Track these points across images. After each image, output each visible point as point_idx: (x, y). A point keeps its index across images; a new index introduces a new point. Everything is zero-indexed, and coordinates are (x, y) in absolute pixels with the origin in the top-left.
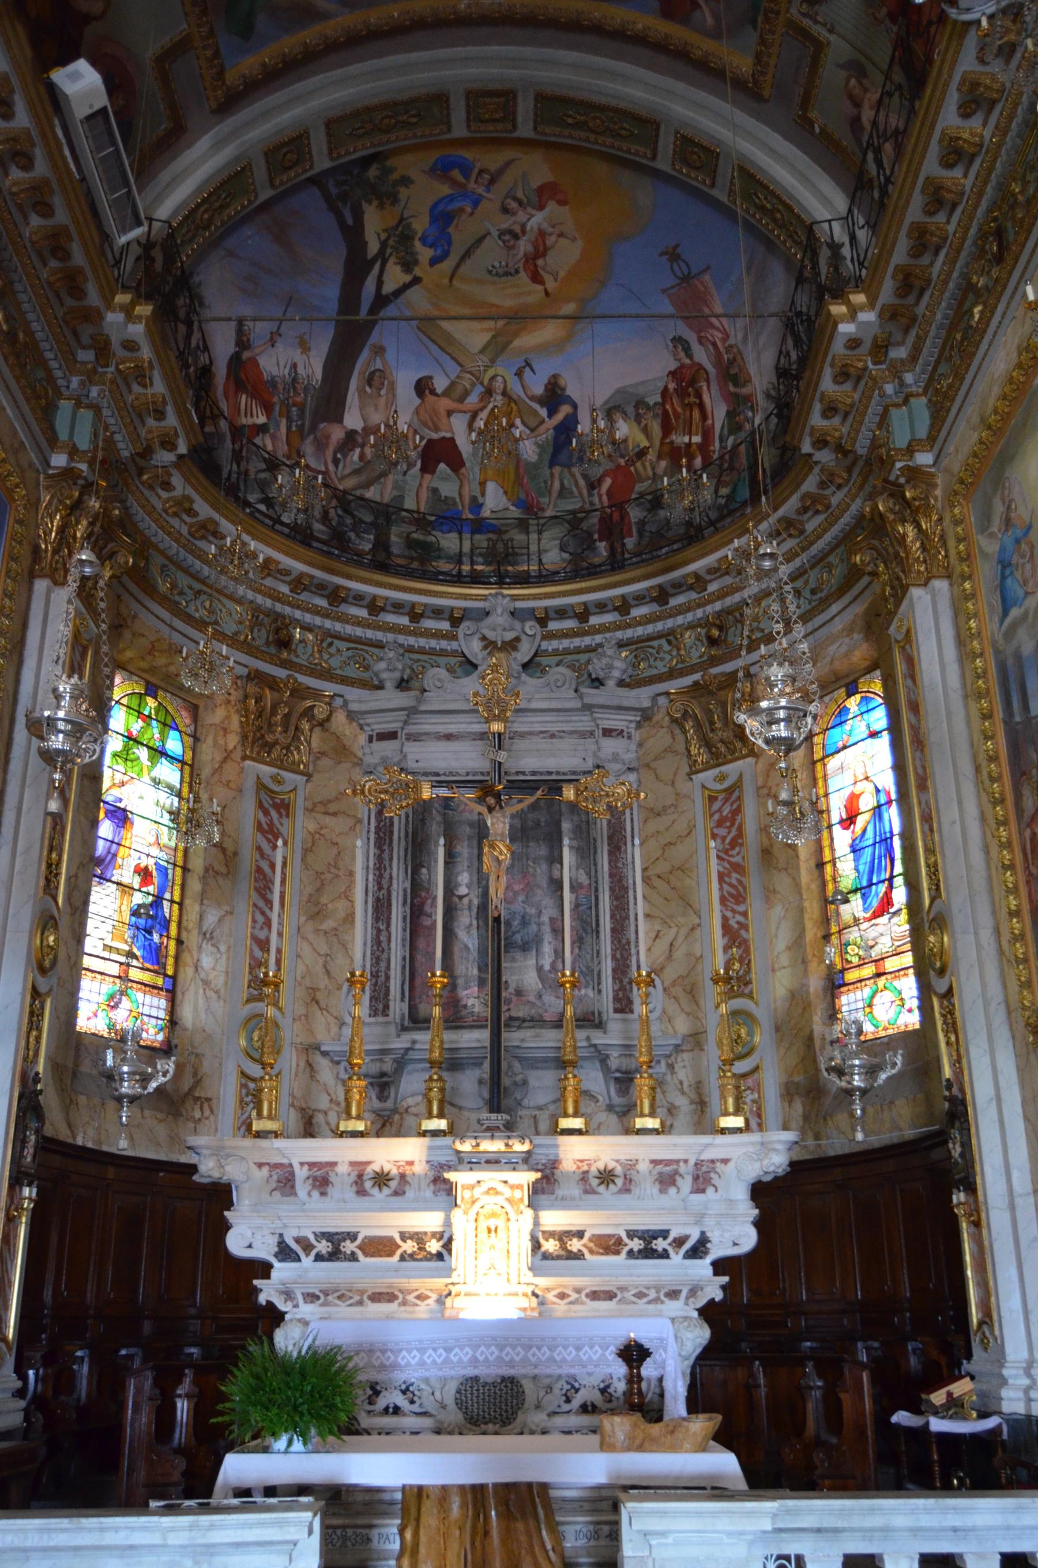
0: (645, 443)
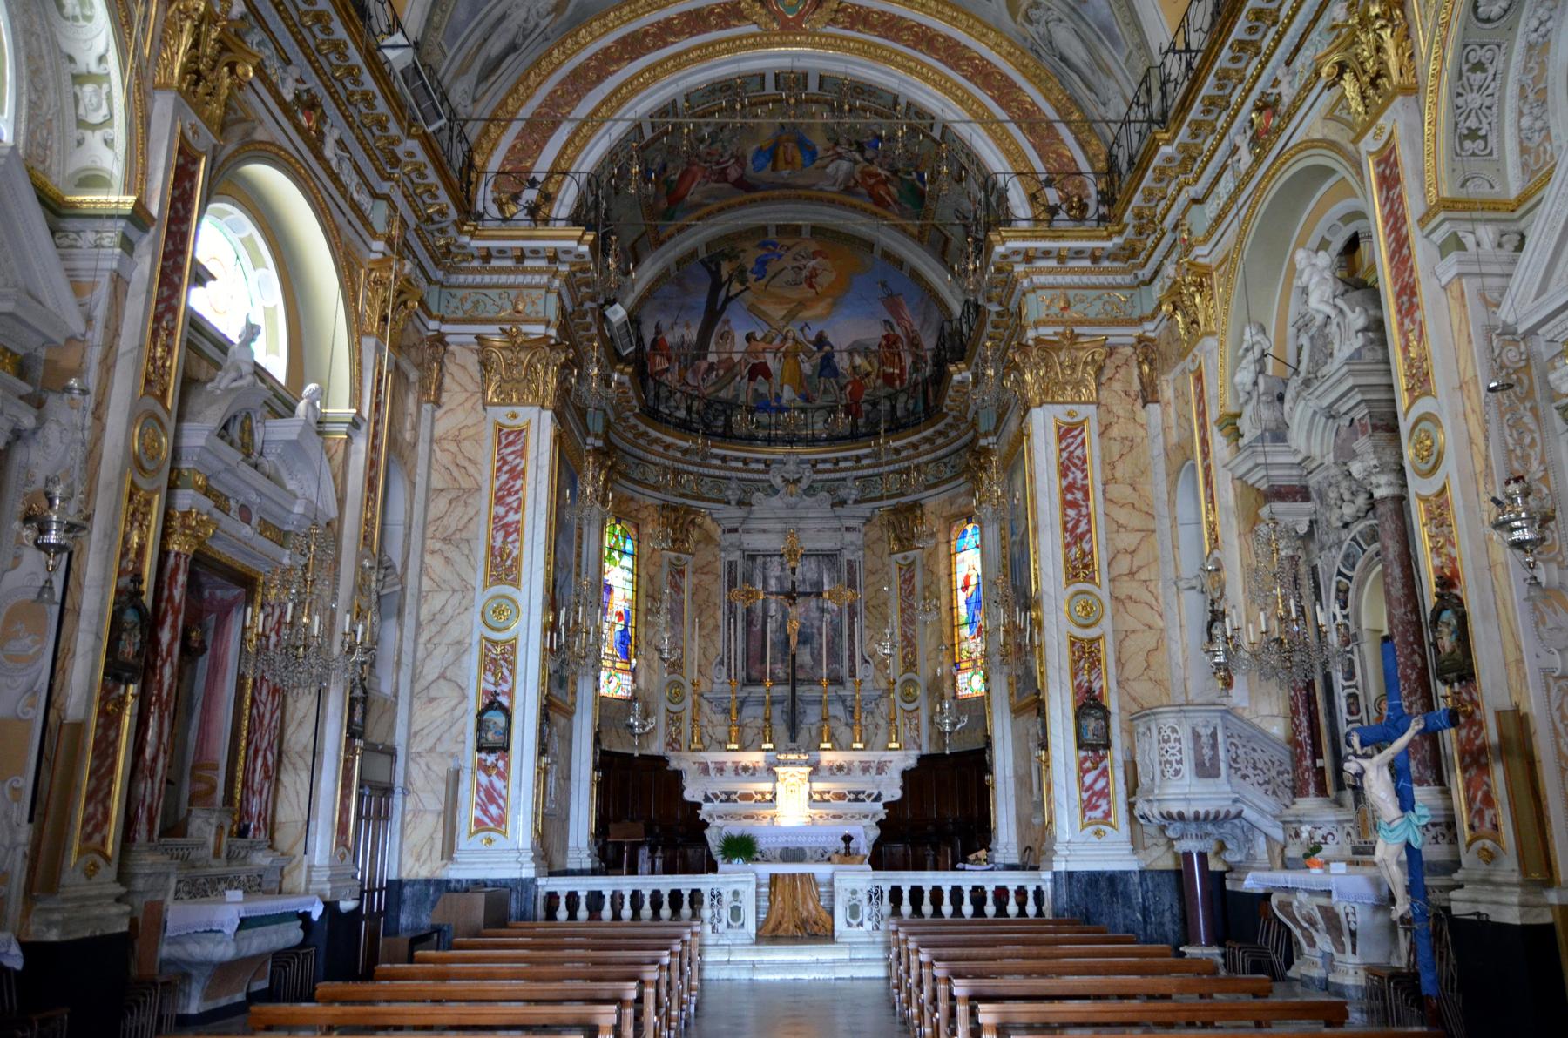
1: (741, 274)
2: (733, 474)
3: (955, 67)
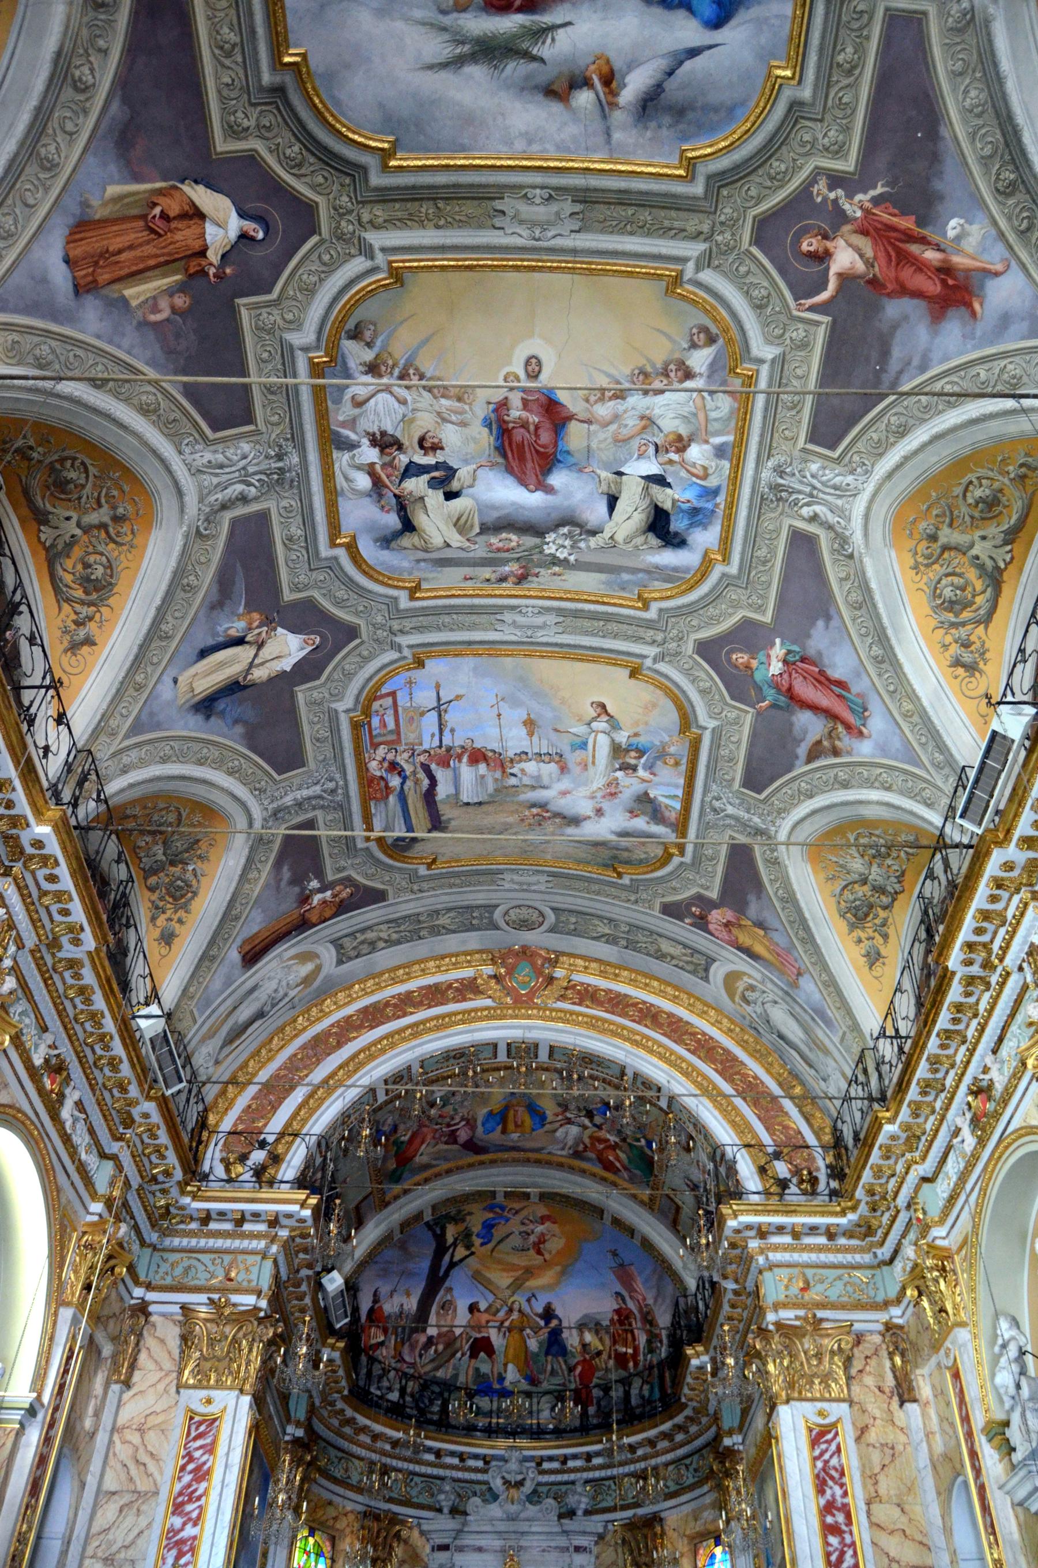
0: (601, 1348)
1: (466, 1238)
2: (448, 1473)
3: (679, 1041)
